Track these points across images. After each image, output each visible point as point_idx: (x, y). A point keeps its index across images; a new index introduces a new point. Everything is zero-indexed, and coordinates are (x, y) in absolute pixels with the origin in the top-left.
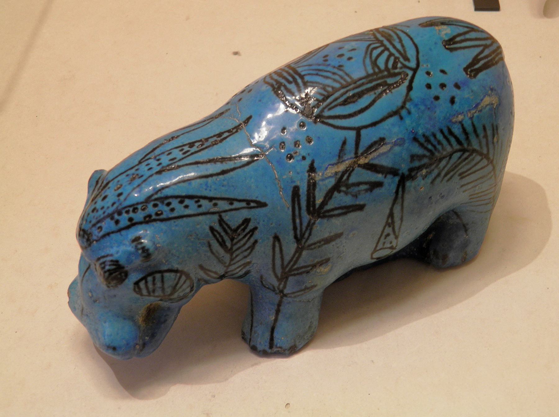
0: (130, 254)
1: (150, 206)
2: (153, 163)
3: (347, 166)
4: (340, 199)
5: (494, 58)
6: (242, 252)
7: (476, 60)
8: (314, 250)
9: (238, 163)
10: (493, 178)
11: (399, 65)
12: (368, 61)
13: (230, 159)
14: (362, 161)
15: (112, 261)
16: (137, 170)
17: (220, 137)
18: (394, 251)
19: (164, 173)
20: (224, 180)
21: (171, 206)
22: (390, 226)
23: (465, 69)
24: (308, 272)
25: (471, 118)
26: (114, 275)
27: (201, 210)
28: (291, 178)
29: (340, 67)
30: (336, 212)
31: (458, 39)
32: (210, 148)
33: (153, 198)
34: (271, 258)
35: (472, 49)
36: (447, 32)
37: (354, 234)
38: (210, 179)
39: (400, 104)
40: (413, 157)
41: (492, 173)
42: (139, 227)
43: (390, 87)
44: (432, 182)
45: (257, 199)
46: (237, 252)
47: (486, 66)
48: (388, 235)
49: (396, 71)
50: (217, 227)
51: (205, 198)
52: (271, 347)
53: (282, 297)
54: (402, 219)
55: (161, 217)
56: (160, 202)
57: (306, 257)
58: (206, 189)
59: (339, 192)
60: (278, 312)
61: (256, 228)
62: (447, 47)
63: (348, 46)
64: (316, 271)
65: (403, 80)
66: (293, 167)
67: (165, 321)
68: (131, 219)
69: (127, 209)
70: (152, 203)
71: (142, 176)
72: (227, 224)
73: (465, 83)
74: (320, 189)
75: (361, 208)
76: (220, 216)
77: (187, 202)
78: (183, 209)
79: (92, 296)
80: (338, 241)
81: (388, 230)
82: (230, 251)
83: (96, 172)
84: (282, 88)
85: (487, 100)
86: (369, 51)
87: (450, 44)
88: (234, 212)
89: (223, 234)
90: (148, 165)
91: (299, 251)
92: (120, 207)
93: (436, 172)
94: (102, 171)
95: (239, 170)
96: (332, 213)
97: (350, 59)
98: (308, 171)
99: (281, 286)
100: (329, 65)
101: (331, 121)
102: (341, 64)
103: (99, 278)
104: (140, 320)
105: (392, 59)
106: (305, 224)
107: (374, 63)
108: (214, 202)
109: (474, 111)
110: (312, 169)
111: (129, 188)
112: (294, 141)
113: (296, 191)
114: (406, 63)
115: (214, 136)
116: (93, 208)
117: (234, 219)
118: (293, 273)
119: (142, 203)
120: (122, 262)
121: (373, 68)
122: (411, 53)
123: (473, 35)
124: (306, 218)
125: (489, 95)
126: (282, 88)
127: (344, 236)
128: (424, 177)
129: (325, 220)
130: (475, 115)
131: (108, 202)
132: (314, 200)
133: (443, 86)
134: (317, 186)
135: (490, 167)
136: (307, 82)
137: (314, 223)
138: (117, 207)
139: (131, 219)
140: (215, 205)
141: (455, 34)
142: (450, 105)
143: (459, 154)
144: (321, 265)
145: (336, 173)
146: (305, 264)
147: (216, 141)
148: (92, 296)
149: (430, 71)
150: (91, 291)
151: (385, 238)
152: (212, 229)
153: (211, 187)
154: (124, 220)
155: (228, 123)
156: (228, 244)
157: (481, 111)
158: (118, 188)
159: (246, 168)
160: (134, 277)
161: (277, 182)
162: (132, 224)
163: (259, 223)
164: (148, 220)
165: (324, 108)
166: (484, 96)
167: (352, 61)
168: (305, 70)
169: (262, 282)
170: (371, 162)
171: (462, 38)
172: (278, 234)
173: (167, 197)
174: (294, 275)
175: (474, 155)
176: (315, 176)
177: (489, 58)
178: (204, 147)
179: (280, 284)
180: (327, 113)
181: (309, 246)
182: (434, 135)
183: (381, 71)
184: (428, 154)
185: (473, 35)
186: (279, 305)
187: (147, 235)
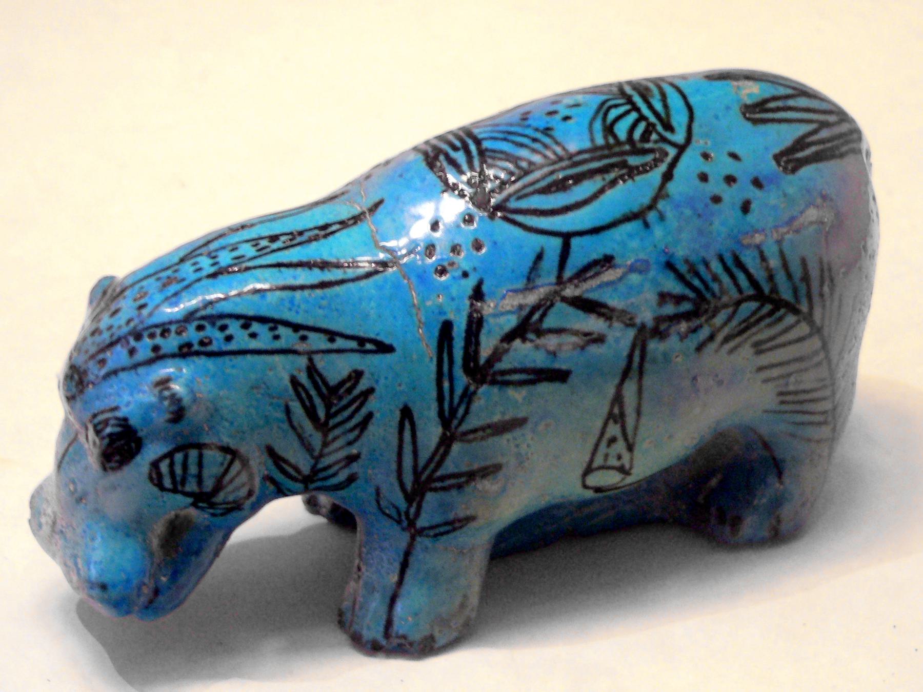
0: (151, 406)
1: (191, 328)
2: (205, 263)
3: (542, 297)
4: (524, 353)
5: (837, 147)
6: (344, 433)
7: (800, 144)
8: (474, 444)
9: (351, 273)
10: (825, 363)
11: (654, 137)
12: (598, 125)
13: (338, 266)
14: (570, 291)
15: (117, 418)
16: (176, 271)
17: (325, 231)
18: (629, 480)
19: (220, 277)
20: (322, 298)
21: (228, 332)
22: (616, 422)
23: (777, 158)
24: (459, 487)
25: (779, 242)
26: (118, 444)
27: (277, 345)
28: (440, 307)
29: (547, 131)
30: (516, 377)
31: (772, 105)
32: (305, 245)
33: (199, 314)
34: (396, 449)
35: (797, 125)
36: (753, 92)
37: (547, 425)
38: (298, 294)
39: (646, 201)
40: (663, 297)
41: (822, 355)
42: (170, 361)
43: (632, 172)
44: (700, 348)
45: (379, 338)
46: (337, 432)
47: (817, 158)
48: (613, 440)
49: (648, 146)
50: (303, 378)
51: (287, 324)
52: (387, 635)
53: (413, 538)
54: (639, 412)
55: (209, 348)
56: (209, 323)
57: (459, 458)
58: (290, 309)
59: (524, 340)
60: (404, 566)
61: (371, 391)
62: (747, 115)
63: (569, 101)
64: (475, 488)
65: (656, 162)
66: (446, 287)
67: (197, 553)
68: (156, 348)
69: (152, 330)
70: (196, 323)
71: (183, 280)
72: (320, 375)
73: (773, 180)
74: (490, 332)
75: (561, 376)
76: (311, 360)
77: (255, 327)
78: (247, 338)
79: (76, 490)
80: (517, 433)
81: (614, 430)
82: (323, 427)
83: (106, 278)
84: (442, 158)
85: (812, 214)
86: (603, 109)
87: (757, 112)
88: (334, 356)
89: (313, 392)
90: (195, 264)
91: (446, 442)
92: (141, 327)
93: (705, 333)
94: (112, 278)
95: (350, 285)
96: (508, 378)
97: (566, 118)
98: (471, 298)
99: (412, 510)
100: (529, 126)
101: (520, 218)
102: (549, 125)
103: (91, 447)
104: (155, 542)
105: (642, 126)
106: (459, 391)
107: (609, 130)
108: (302, 333)
109: (785, 230)
110: (478, 294)
111: (158, 297)
112: (451, 244)
113: (447, 327)
114: (668, 135)
115: (316, 228)
116: (93, 328)
117: (336, 368)
118: (434, 485)
119: (178, 322)
120: (133, 422)
121: (605, 137)
122: (679, 119)
123: (802, 102)
124: (462, 379)
125: (818, 207)
126: (442, 158)
127: (529, 426)
128: (683, 337)
129: (495, 390)
130: (787, 237)
131: (120, 319)
132: (477, 352)
133: (730, 180)
134: (485, 324)
135: (816, 342)
136: (487, 150)
137: (475, 393)
138: (135, 328)
139: (156, 348)
140: (304, 338)
141: (767, 95)
142: (740, 213)
143: (753, 305)
144: (484, 476)
145: (521, 307)
146: (456, 470)
147: (318, 235)
148: (76, 490)
149: (708, 151)
150: (74, 482)
151: (609, 446)
152: (294, 382)
153: (299, 306)
154: (144, 349)
155: (344, 211)
156: (321, 413)
157: (797, 231)
158: (141, 297)
159: (363, 283)
160: (152, 451)
161: (414, 311)
162: (158, 356)
163: (377, 382)
164: (185, 352)
165: (510, 196)
166: (808, 206)
167: (570, 122)
168: (485, 132)
169: (378, 502)
170: (586, 296)
171: (780, 104)
172: (410, 405)
173: (222, 316)
174: (435, 490)
175: (782, 311)
176: (482, 307)
177: (829, 145)
178: (294, 242)
179: (410, 505)
180: (513, 204)
181: (465, 434)
182: (707, 264)
183: (618, 143)
184: (692, 295)
185: (802, 102)
186: (407, 554)
187: (182, 377)
